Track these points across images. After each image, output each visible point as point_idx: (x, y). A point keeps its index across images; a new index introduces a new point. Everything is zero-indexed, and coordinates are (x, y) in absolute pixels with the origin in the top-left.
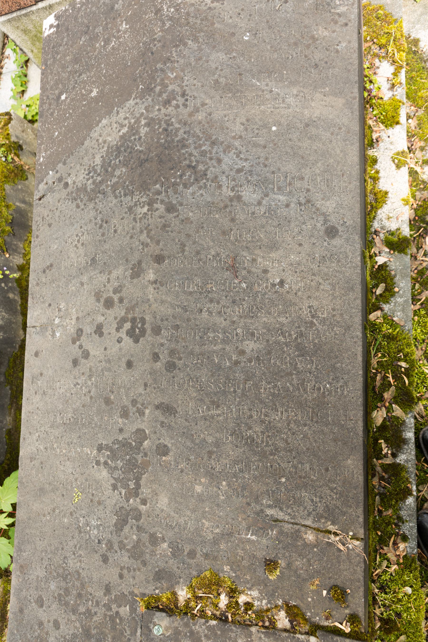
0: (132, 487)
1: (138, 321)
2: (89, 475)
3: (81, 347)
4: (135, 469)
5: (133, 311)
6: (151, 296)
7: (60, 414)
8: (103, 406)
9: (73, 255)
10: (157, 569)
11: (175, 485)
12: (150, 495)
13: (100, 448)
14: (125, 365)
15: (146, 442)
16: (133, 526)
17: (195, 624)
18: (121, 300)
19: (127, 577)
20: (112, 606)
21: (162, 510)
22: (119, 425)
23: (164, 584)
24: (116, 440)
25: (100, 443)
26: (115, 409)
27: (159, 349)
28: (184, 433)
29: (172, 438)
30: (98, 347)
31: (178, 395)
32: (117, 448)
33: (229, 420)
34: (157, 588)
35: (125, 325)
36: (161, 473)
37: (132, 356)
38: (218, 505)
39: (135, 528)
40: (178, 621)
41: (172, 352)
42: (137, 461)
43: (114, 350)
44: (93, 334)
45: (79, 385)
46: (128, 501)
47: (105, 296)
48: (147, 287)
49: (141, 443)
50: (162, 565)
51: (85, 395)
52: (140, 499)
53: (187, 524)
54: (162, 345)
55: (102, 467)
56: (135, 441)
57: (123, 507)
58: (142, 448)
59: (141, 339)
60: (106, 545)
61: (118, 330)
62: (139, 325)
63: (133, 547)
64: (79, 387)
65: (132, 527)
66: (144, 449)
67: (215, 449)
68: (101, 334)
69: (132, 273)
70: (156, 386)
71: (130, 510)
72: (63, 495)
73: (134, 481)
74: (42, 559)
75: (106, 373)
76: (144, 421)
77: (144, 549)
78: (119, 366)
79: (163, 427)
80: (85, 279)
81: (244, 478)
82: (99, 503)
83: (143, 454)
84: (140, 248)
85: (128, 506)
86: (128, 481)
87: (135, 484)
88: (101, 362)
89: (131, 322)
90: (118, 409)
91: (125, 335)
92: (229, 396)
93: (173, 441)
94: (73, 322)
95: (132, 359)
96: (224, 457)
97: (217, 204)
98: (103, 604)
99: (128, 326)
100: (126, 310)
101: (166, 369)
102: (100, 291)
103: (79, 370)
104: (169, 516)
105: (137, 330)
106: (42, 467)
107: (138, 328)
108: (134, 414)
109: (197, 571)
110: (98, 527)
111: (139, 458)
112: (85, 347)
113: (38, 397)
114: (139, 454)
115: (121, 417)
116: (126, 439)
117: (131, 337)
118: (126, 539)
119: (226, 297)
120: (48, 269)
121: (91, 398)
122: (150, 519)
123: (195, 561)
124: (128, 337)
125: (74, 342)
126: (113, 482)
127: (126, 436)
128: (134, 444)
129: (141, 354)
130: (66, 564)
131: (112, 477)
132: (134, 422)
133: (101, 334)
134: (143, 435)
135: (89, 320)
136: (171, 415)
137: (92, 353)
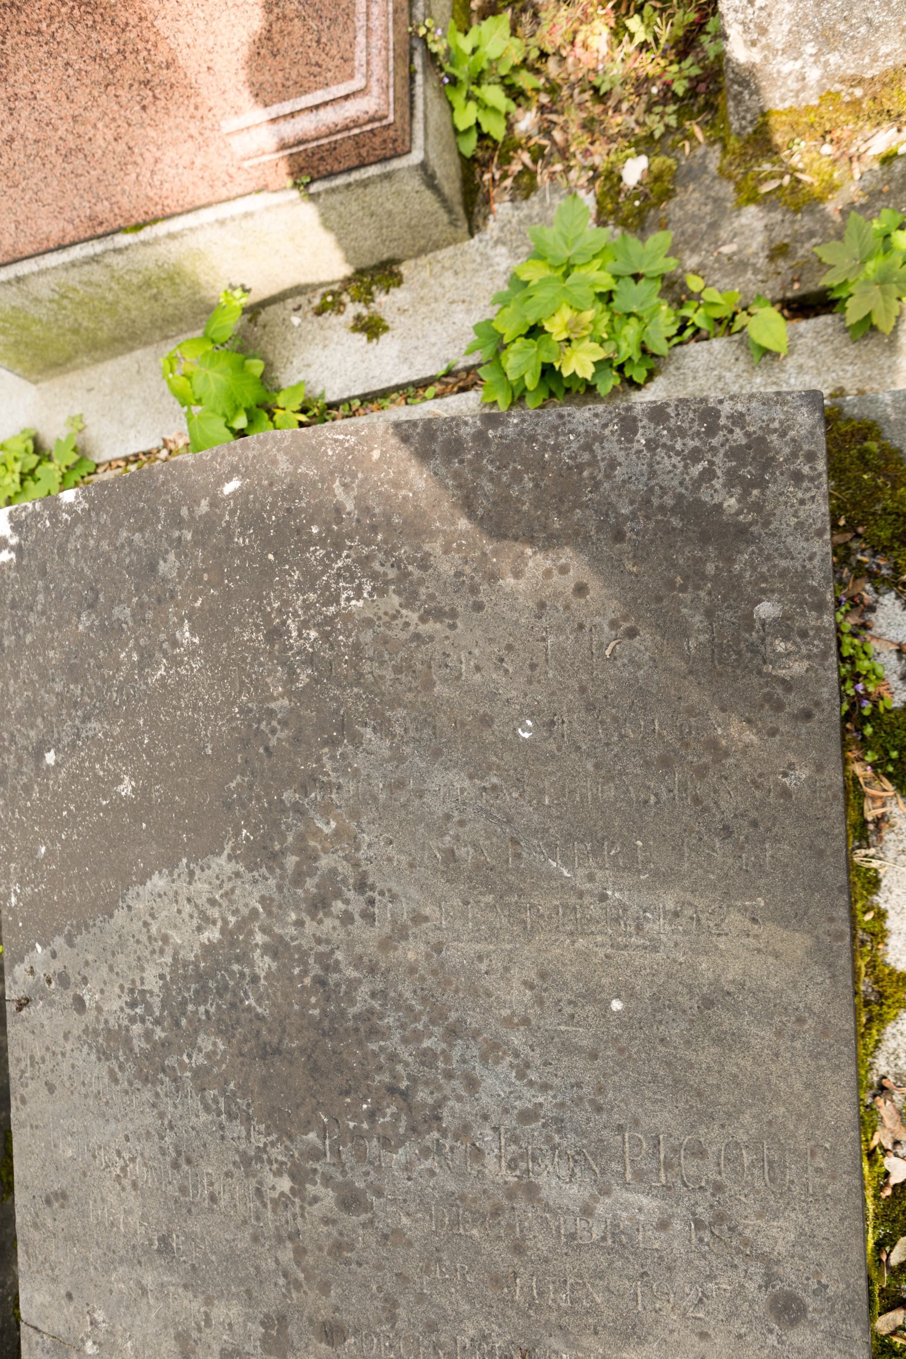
97: (474, 1200)
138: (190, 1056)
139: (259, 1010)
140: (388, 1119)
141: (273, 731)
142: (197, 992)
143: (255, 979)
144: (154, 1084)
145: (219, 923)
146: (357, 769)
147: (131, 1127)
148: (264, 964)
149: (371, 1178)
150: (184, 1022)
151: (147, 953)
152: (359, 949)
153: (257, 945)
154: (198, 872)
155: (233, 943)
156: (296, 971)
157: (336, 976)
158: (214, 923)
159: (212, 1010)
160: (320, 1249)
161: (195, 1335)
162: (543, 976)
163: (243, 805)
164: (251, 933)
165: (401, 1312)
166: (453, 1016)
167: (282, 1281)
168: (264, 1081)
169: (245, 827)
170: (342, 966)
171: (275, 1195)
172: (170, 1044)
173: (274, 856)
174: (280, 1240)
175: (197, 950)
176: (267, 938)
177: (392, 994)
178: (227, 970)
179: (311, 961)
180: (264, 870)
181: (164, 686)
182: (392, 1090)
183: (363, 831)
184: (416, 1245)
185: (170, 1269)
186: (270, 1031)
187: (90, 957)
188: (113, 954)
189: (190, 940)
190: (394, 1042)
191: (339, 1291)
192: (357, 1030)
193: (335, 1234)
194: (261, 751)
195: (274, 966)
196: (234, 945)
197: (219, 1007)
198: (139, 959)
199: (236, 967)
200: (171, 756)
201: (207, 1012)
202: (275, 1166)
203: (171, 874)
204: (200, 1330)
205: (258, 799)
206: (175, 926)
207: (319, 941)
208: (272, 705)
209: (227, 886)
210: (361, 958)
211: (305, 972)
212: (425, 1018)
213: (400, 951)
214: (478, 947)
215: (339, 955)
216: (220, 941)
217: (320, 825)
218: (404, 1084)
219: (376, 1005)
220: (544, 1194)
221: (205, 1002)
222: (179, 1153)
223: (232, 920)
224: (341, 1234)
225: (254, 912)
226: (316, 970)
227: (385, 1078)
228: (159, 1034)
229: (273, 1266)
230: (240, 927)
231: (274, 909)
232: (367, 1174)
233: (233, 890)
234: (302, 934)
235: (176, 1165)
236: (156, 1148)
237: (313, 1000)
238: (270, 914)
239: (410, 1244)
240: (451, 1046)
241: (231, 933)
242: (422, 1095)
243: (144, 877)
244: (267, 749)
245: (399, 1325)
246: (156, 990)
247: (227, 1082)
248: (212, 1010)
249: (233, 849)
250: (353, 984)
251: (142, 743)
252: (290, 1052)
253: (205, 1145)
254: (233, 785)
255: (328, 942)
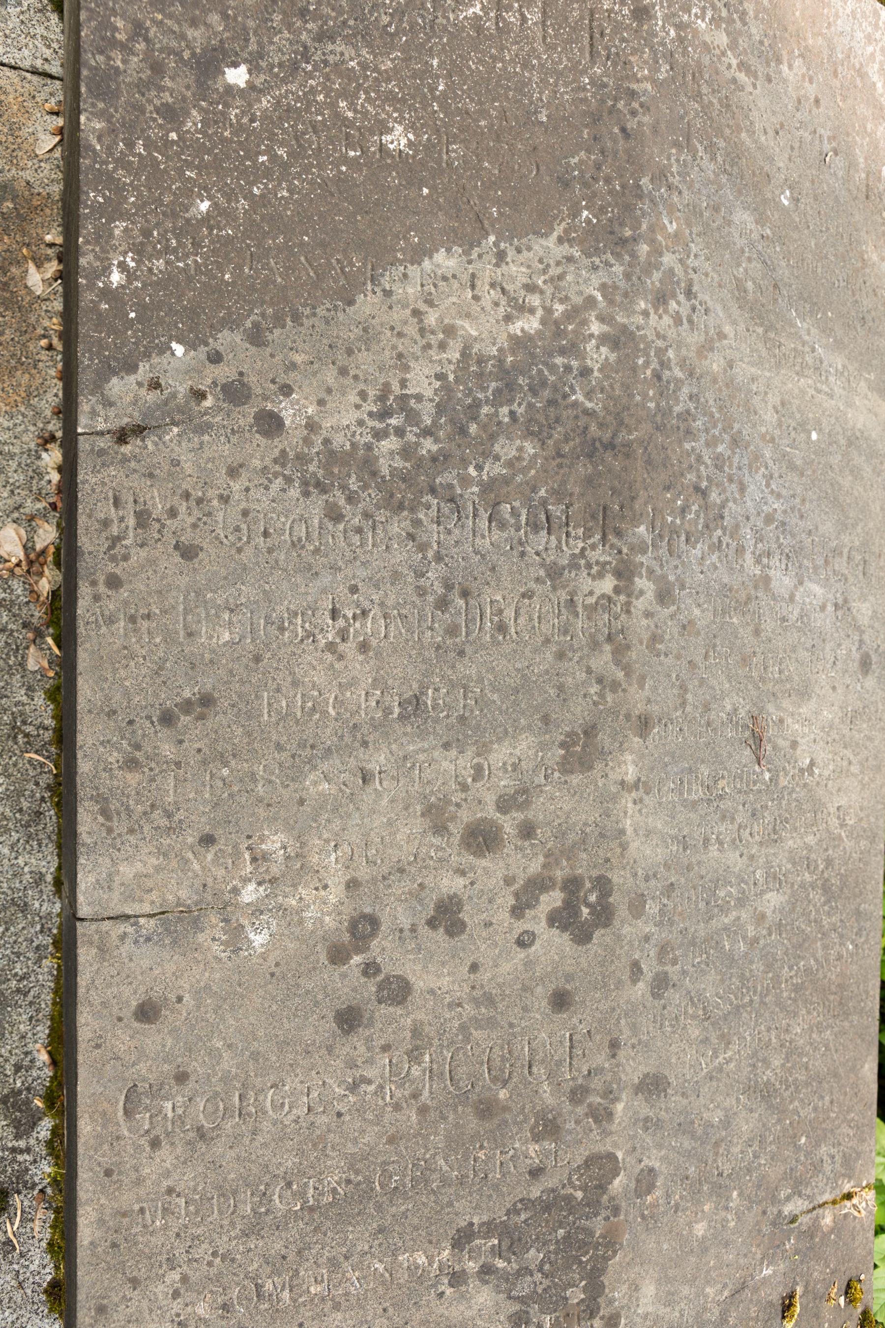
138: (479, 468)
139: (589, 405)
140: (692, 516)
141: (634, 113)
142: (498, 392)
143: (585, 372)
144: (412, 510)
145: (540, 312)
146: (692, 181)
147: (362, 573)
148: (598, 356)
149: (679, 571)
150: (473, 428)
151: (417, 349)
152: (684, 352)
153: (592, 336)
154: (511, 254)
155: (559, 333)
156: (640, 361)
157: (667, 372)
158: (532, 311)
159: (521, 410)
162: (783, 404)
163: (586, 185)
164: (585, 323)
165: (689, 696)
166: (736, 426)
168: (589, 482)
169: (587, 208)
170: (673, 365)
171: (592, 600)
172: (446, 457)
173: (623, 242)
175: (503, 341)
176: (606, 328)
177: (702, 400)
178: (546, 364)
179: (652, 354)
180: (609, 256)
181: (479, 29)
182: (697, 489)
183: (693, 241)
184: (702, 632)
186: (601, 426)
187: (299, 358)
188: (350, 352)
189: (487, 330)
190: (699, 445)
191: (651, 683)
192: (678, 428)
193: (653, 626)
194: (616, 130)
195: (613, 357)
196: (562, 336)
197: (530, 406)
198: (400, 356)
199: (559, 361)
200: (483, 113)
201: (512, 413)
202: (595, 569)
203: (467, 253)
205: (608, 180)
206: (468, 315)
207: (658, 335)
208: (634, 86)
209: (554, 271)
210: (685, 361)
211: (647, 363)
212: (720, 426)
213: (708, 361)
214: (753, 370)
215: (671, 354)
216: (539, 332)
217: (666, 222)
218: (704, 484)
219: (692, 406)
220: (773, 584)
221: (510, 402)
222: (449, 587)
223: (559, 309)
224: (656, 626)
225: (590, 301)
226: (655, 365)
227: (691, 477)
228: (429, 446)
229: (582, 676)
230: (568, 316)
231: (618, 298)
232: (676, 567)
233: (561, 277)
234: (647, 324)
235: (443, 604)
236: (410, 589)
237: (651, 393)
238: (611, 302)
240: (734, 453)
241: (556, 323)
242: (714, 497)
243: (417, 255)
244: (623, 130)
245: (689, 709)
246: (428, 393)
247: (534, 489)
248: (521, 410)
249: (566, 231)
250: (679, 382)
251: (433, 89)
252: (628, 445)
253: (493, 569)
254: (574, 160)
255: (664, 338)
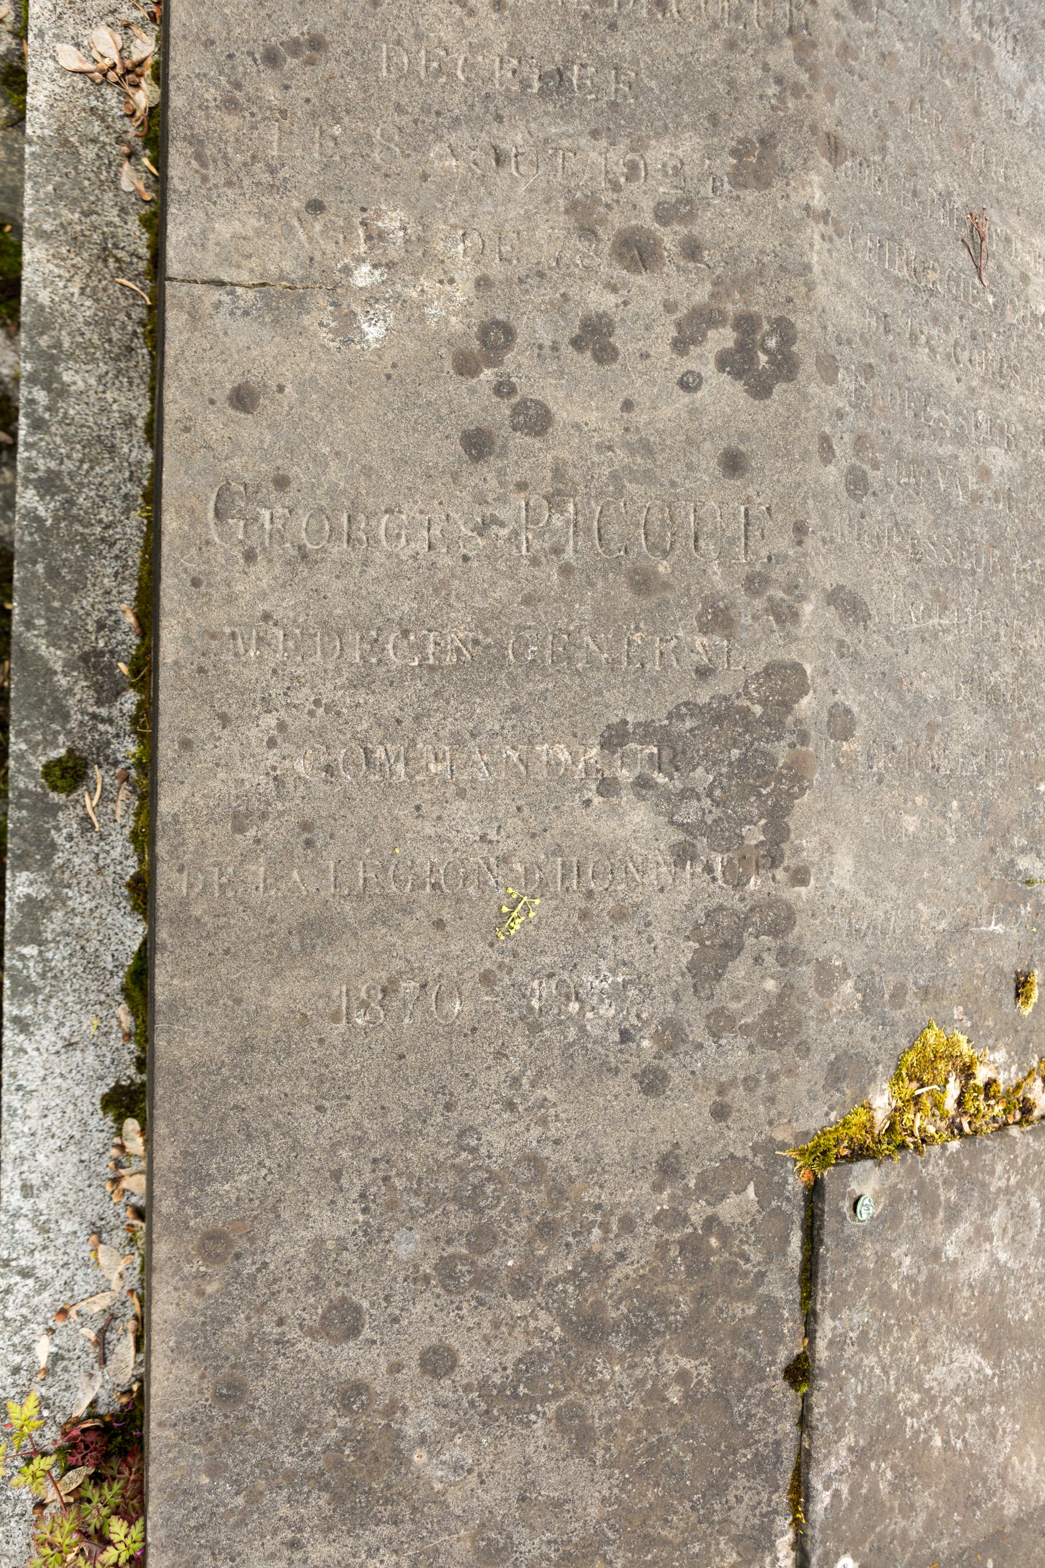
0: (754, 842)
1: (766, 327)
2: (567, 834)
3: (504, 389)
4: (767, 784)
5: (742, 292)
6: (815, 258)
7: (405, 633)
8: (626, 597)
9: (447, 33)
10: (832, 1056)
11: (866, 819)
12: (817, 853)
13: (614, 739)
14: (713, 463)
15: (805, 701)
16: (765, 955)
17: (926, 1163)
18: (692, 250)
19: (746, 1105)
20: (690, 1211)
21: (842, 893)
22: (696, 658)
23: (847, 1091)
24: (686, 704)
25: (615, 720)
26: (679, 606)
27: (834, 427)
28: (884, 674)
29: (860, 690)
30: (591, 395)
31: (871, 567)
32: (691, 730)
33: (963, 644)
34: (832, 1108)
35: (711, 334)
36: (838, 789)
37: (744, 437)
38: (944, 862)
39: (769, 959)
40: (896, 1167)
41: (860, 442)
42: (773, 761)
43: (666, 412)
44: (567, 351)
45: (502, 525)
46: (739, 884)
47: (617, 221)
48: (798, 226)
49: (787, 706)
50: (841, 1040)
51: (535, 562)
52: (786, 869)
53: (889, 920)
54: (840, 415)
55: (626, 797)
56: (764, 702)
57: (721, 908)
58: (790, 719)
59: (778, 388)
60: (657, 1037)
61: (681, 345)
62: (772, 343)
63: (769, 1013)
64: (504, 532)
65: (758, 960)
66: (798, 722)
67: (940, 719)
68: (605, 354)
69: (736, 167)
70: (827, 535)
71: (752, 910)
72: (439, 924)
73: (763, 822)
74: (337, 1175)
75: (631, 487)
76: (797, 639)
77: (804, 1008)
78: (690, 467)
79: (842, 656)
80: (514, 138)
81: (987, 787)
82: (620, 915)
83: (794, 738)
84: (770, 92)
85: (742, 899)
86: (740, 825)
87: (765, 830)
88: (610, 448)
89: (736, 326)
90: (690, 605)
91: (712, 366)
92: (964, 583)
93: (863, 698)
94: (462, 291)
95: (742, 448)
96: (955, 737)
97: (950, 47)
98: (649, 1216)
99: (722, 338)
100: (715, 284)
101: (848, 490)
102: (597, 201)
103: (501, 473)
104: (855, 905)
105: (763, 358)
106: (309, 843)
107: (766, 351)
108: (755, 617)
109: (908, 1035)
110: (618, 993)
111: (782, 751)
112: (524, 389)
113: (262, 574)
114: (779, 738)
115: (705, 629)
116: (726, 699)
117: (737, 374)
118: (737, 998)
119: (961, 318)
120: (295, 54)
121: (566, 570)
122: (817, 922)
123: (903, 1011)
124: (725, 377)
125: (466, 366)
126: (679, 836)
127: (724, 688)
128: (758, 710)
129: (778, 433)
130: (473, 1150)
131: (672, 823)
132: (756, 643)
133: (605, 354)
134: (795, 679)
135: (543, 294)
136: (857, 622)
137: (563, 414)
160: (830, 47)
161: (607, 197)
167: (772, 90)
174: (773, 38)
185: (566, 115)
204: (616, 187)
239: (901, 73)
